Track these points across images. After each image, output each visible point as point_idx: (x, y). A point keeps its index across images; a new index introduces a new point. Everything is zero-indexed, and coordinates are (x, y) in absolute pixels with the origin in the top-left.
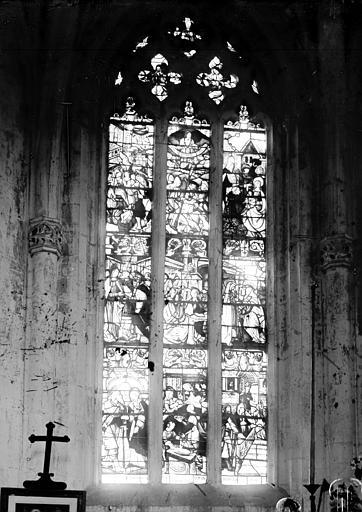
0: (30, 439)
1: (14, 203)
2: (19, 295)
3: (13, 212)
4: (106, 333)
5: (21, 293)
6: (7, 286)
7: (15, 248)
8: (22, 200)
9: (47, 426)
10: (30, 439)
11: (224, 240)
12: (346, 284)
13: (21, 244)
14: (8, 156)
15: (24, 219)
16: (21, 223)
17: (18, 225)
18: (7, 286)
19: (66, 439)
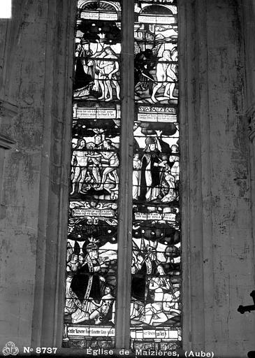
0: (239, 310)
1: (231, 102)
2: (243, 181)
3: (231, 111)
4: (99, 189)
5: (245, 178)
6: (229, 175)
7: (235, 141)
8: (239, 98)
9: (242, 313)
10: (239, 310)
11: (69, 199)
12: (50, 110)
13: (241, 135)
14: (222, 67)
15: (243, 114)
16: (240, 118)
17: (238, 121)
18: (229, 175)
19: (242, 309)
